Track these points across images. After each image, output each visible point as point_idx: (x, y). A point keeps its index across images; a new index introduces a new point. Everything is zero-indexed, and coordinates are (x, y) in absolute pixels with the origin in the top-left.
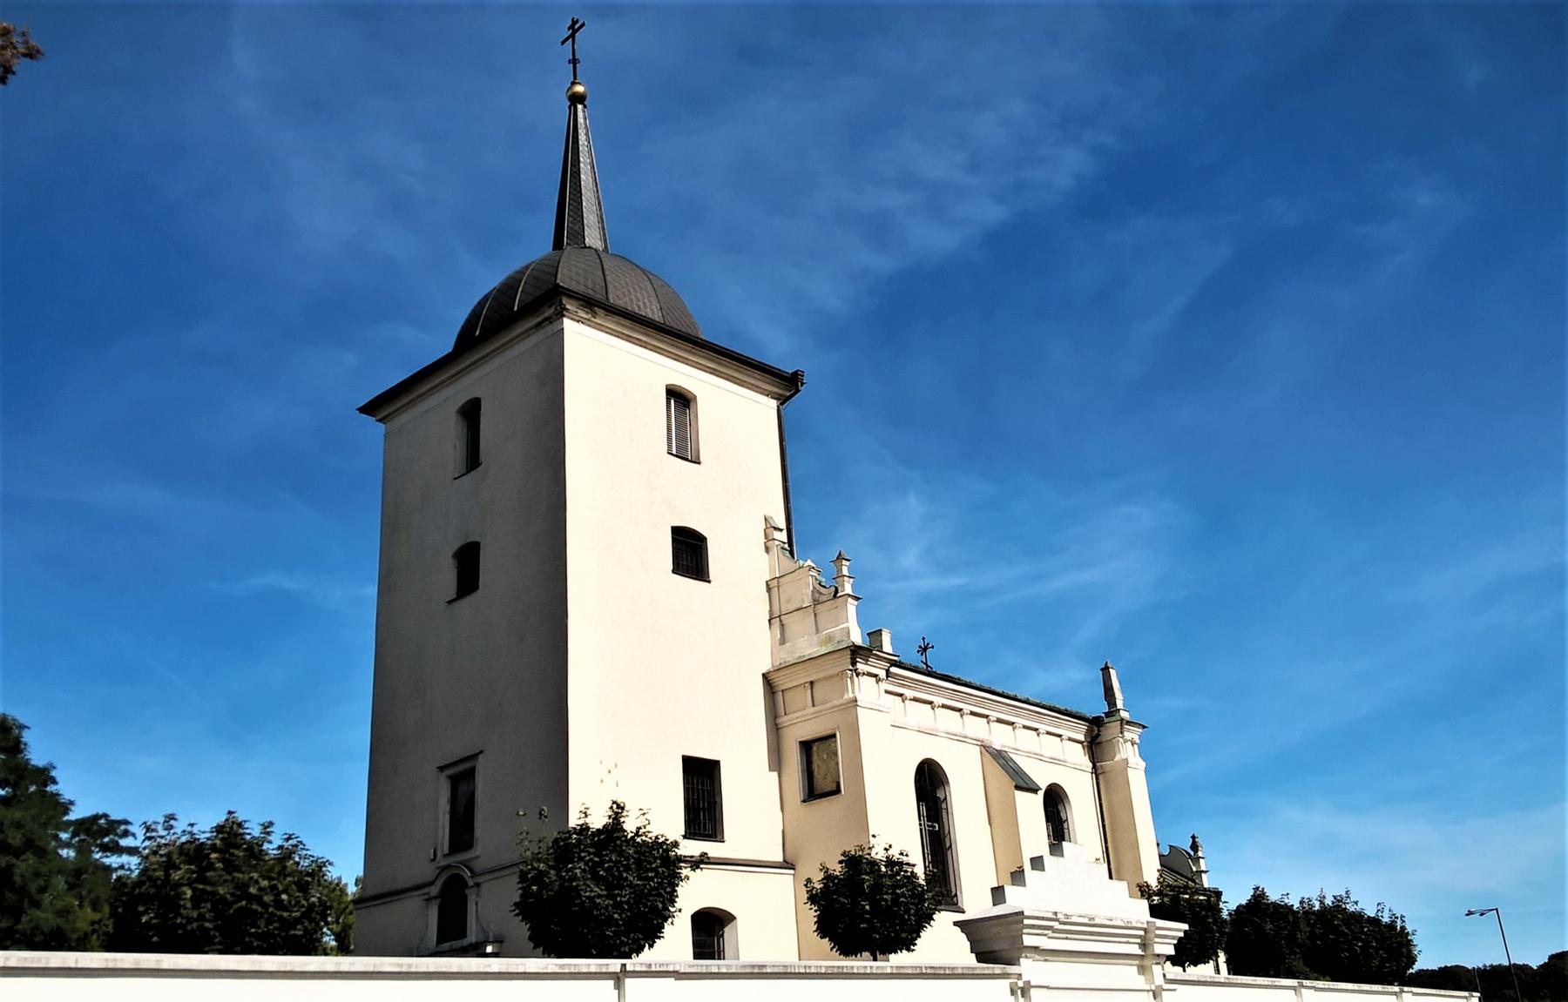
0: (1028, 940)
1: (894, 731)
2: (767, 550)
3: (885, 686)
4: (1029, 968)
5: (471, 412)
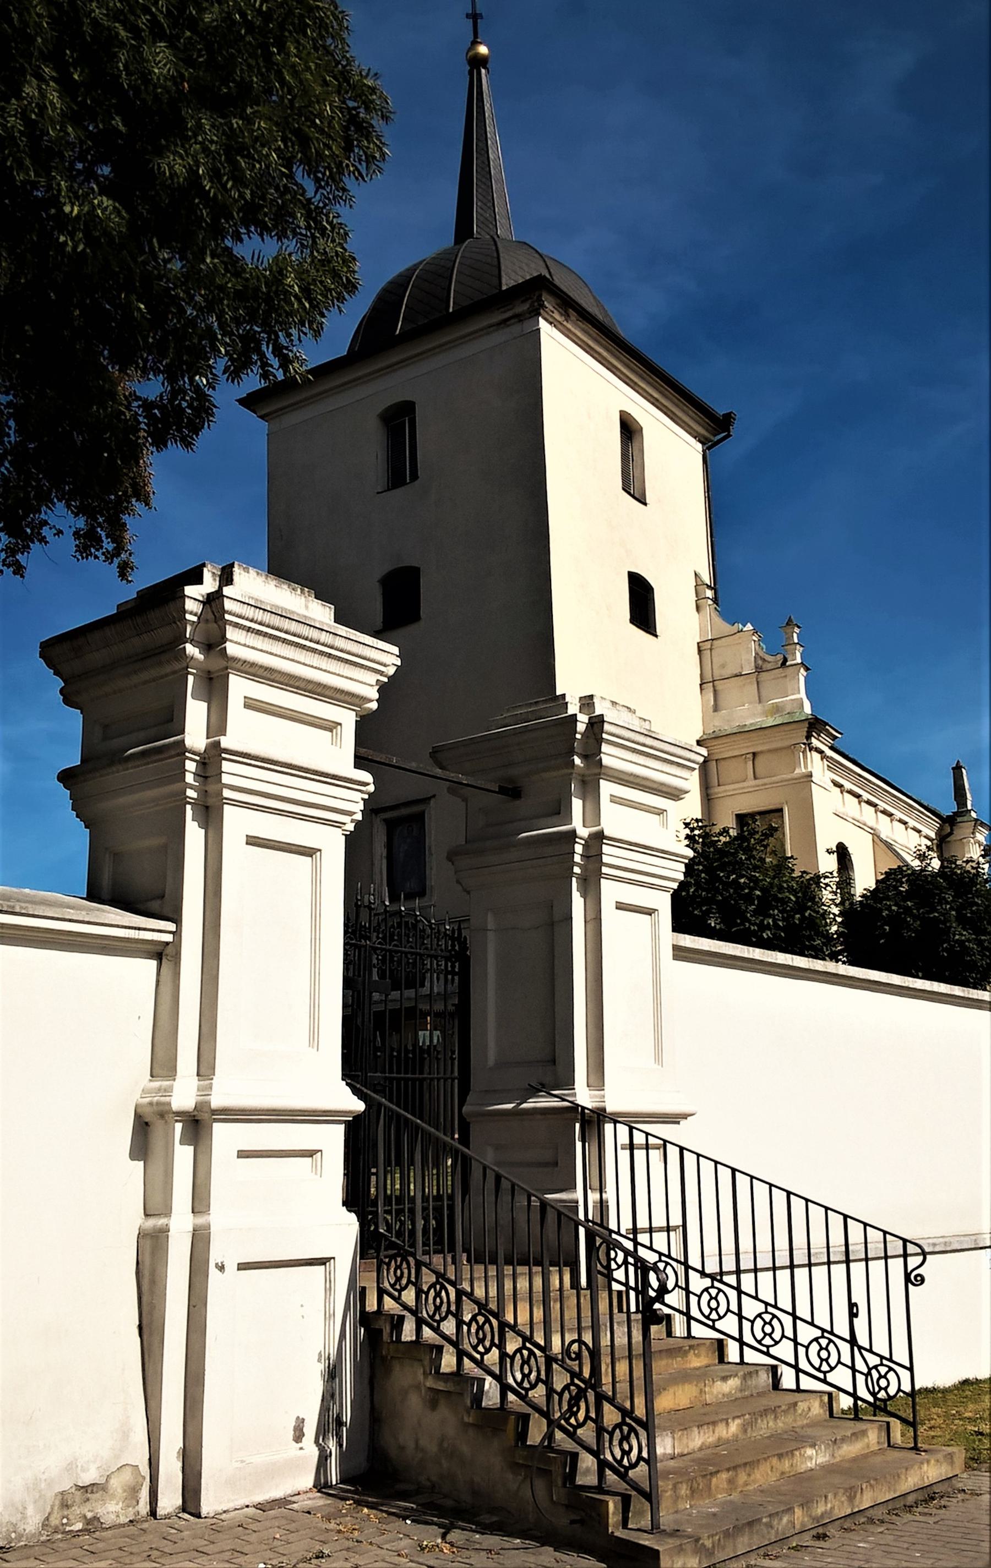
2: (698, 608)
5: (399, 420)
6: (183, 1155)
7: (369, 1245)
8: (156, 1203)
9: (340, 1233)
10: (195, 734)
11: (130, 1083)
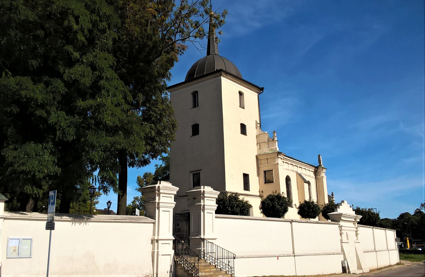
0: (342, 218)
1: (285, 169)
2: (256, 128)
3: (282, 160)
4: (341, 223)
5: (195, 94)
6: (156, 244)
7: (176, 254)
8: (153, 249)
9: (172, 252)
10: (157, 201)
11: (150, 236)
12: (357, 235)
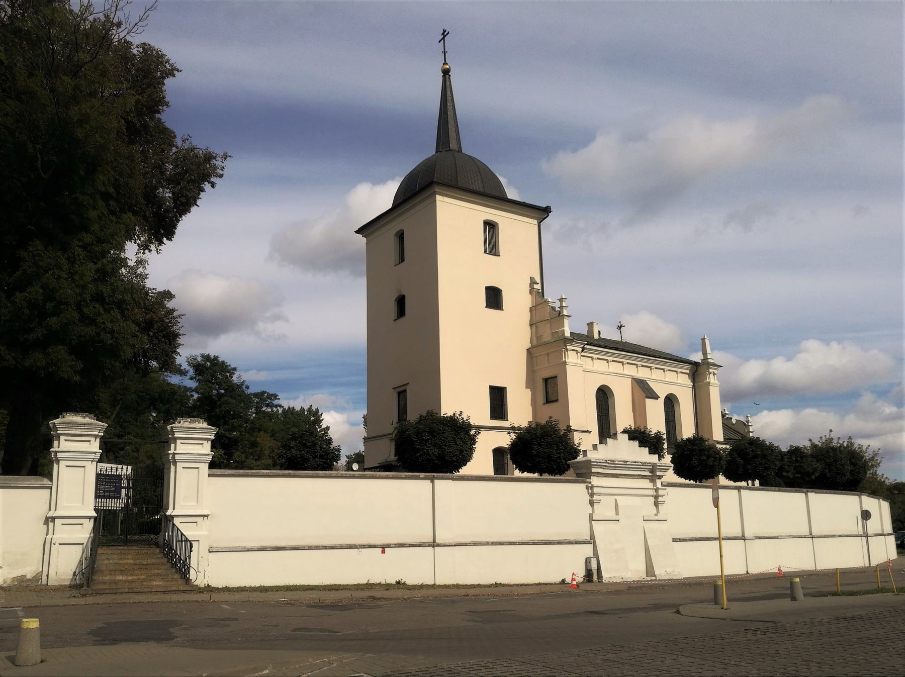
12: (656, 504)
